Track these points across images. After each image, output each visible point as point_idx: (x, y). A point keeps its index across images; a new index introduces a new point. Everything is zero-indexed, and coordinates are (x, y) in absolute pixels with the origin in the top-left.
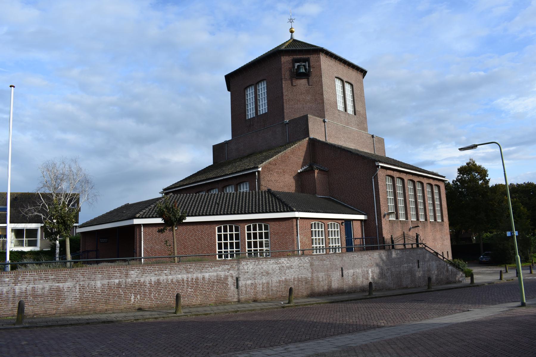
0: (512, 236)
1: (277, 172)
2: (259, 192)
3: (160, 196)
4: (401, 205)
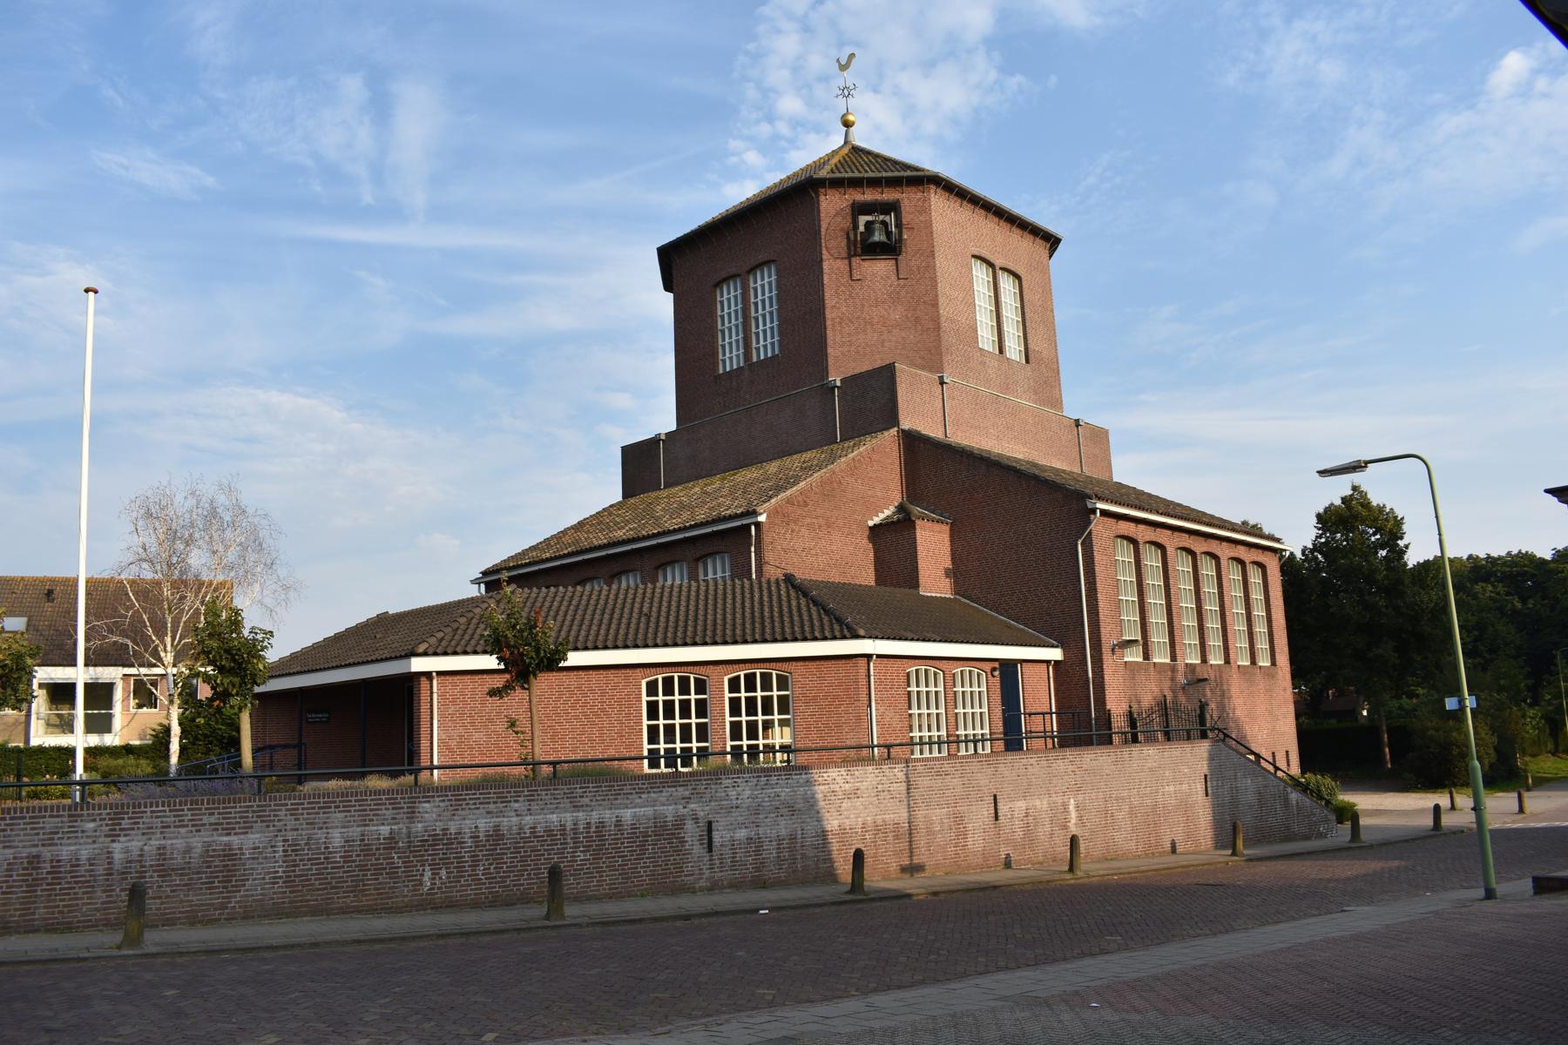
0: (1462, 708)
1: (810, 526)
2: (760, 583)
3: (474, 591)
4: (1157, 619)
